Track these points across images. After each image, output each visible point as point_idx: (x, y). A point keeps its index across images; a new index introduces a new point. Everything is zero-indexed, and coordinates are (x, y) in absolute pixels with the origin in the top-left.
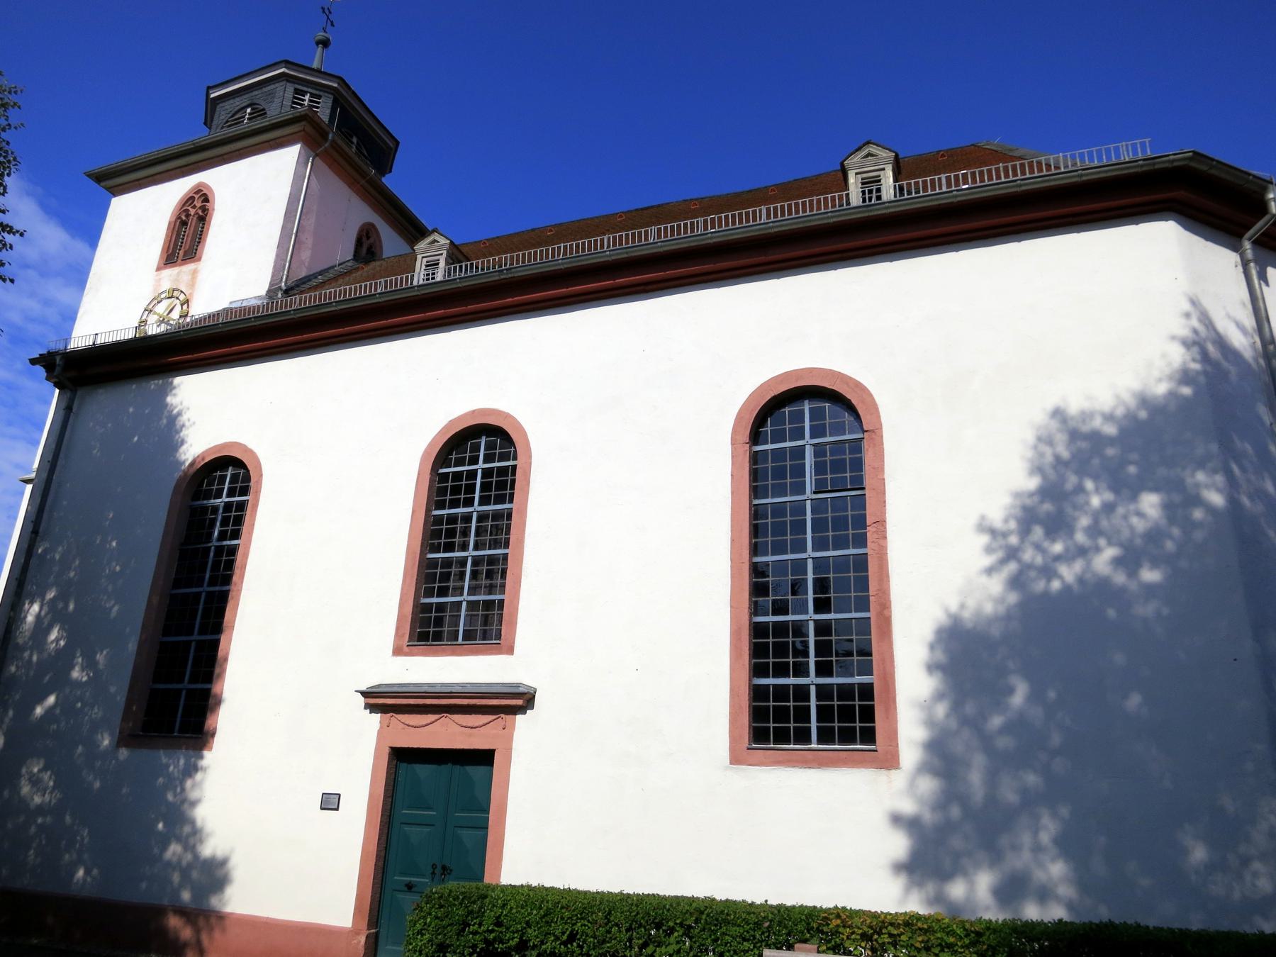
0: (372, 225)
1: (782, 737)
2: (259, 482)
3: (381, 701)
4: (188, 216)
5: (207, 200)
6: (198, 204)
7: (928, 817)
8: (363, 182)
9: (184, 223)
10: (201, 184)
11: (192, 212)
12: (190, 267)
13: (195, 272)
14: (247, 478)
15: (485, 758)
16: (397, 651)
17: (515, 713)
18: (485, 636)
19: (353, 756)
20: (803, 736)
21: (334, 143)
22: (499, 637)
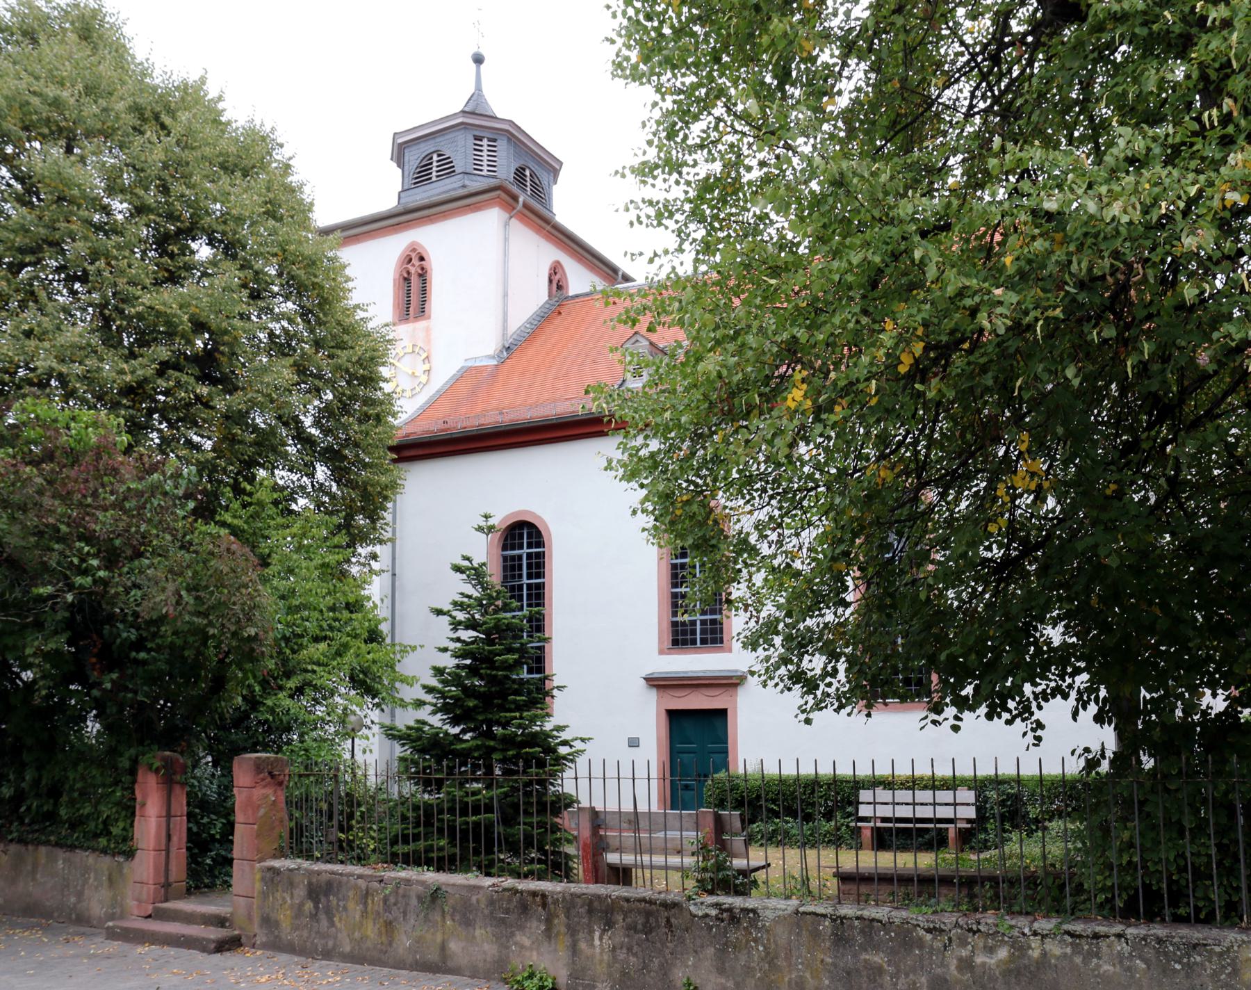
0: (558, 262)
1: (685, 643)
2: (550, 540)
3: (659, 684)
4: (409, 273)
5: (422, 259)
6: (415, 261)
7: (862, 703)
8: (548, 228)
9: (407, 280)
10: (413, 243)
11: (413, 270)
12: (421, 324)
13: (428, 330)
14: (539, 534)
15: (723, 713)
16: (661, 652)
17: (401, 209)
18: (714, 641)
19: (646, 720)
20: (694, 642)
21: (525, 206)
22: (722, 642)
